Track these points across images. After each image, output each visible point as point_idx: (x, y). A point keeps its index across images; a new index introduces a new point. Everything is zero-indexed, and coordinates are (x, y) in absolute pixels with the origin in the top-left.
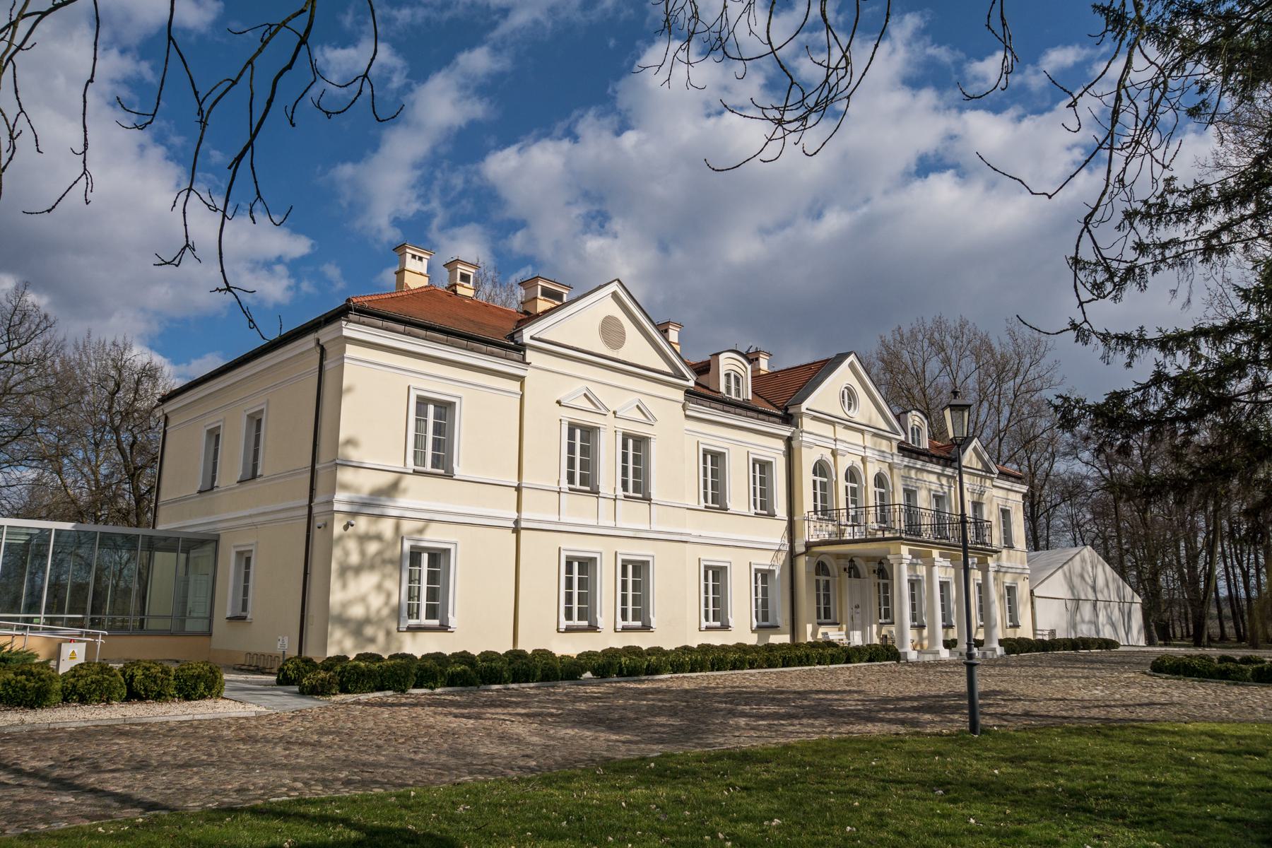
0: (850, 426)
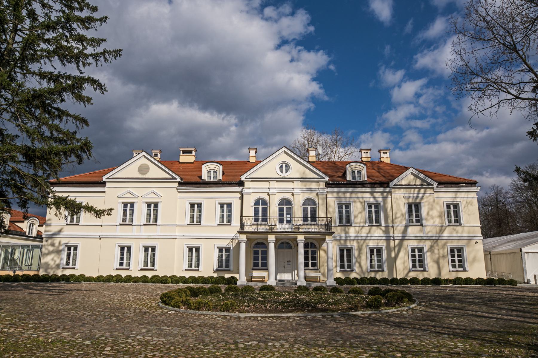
0: (291, 180)
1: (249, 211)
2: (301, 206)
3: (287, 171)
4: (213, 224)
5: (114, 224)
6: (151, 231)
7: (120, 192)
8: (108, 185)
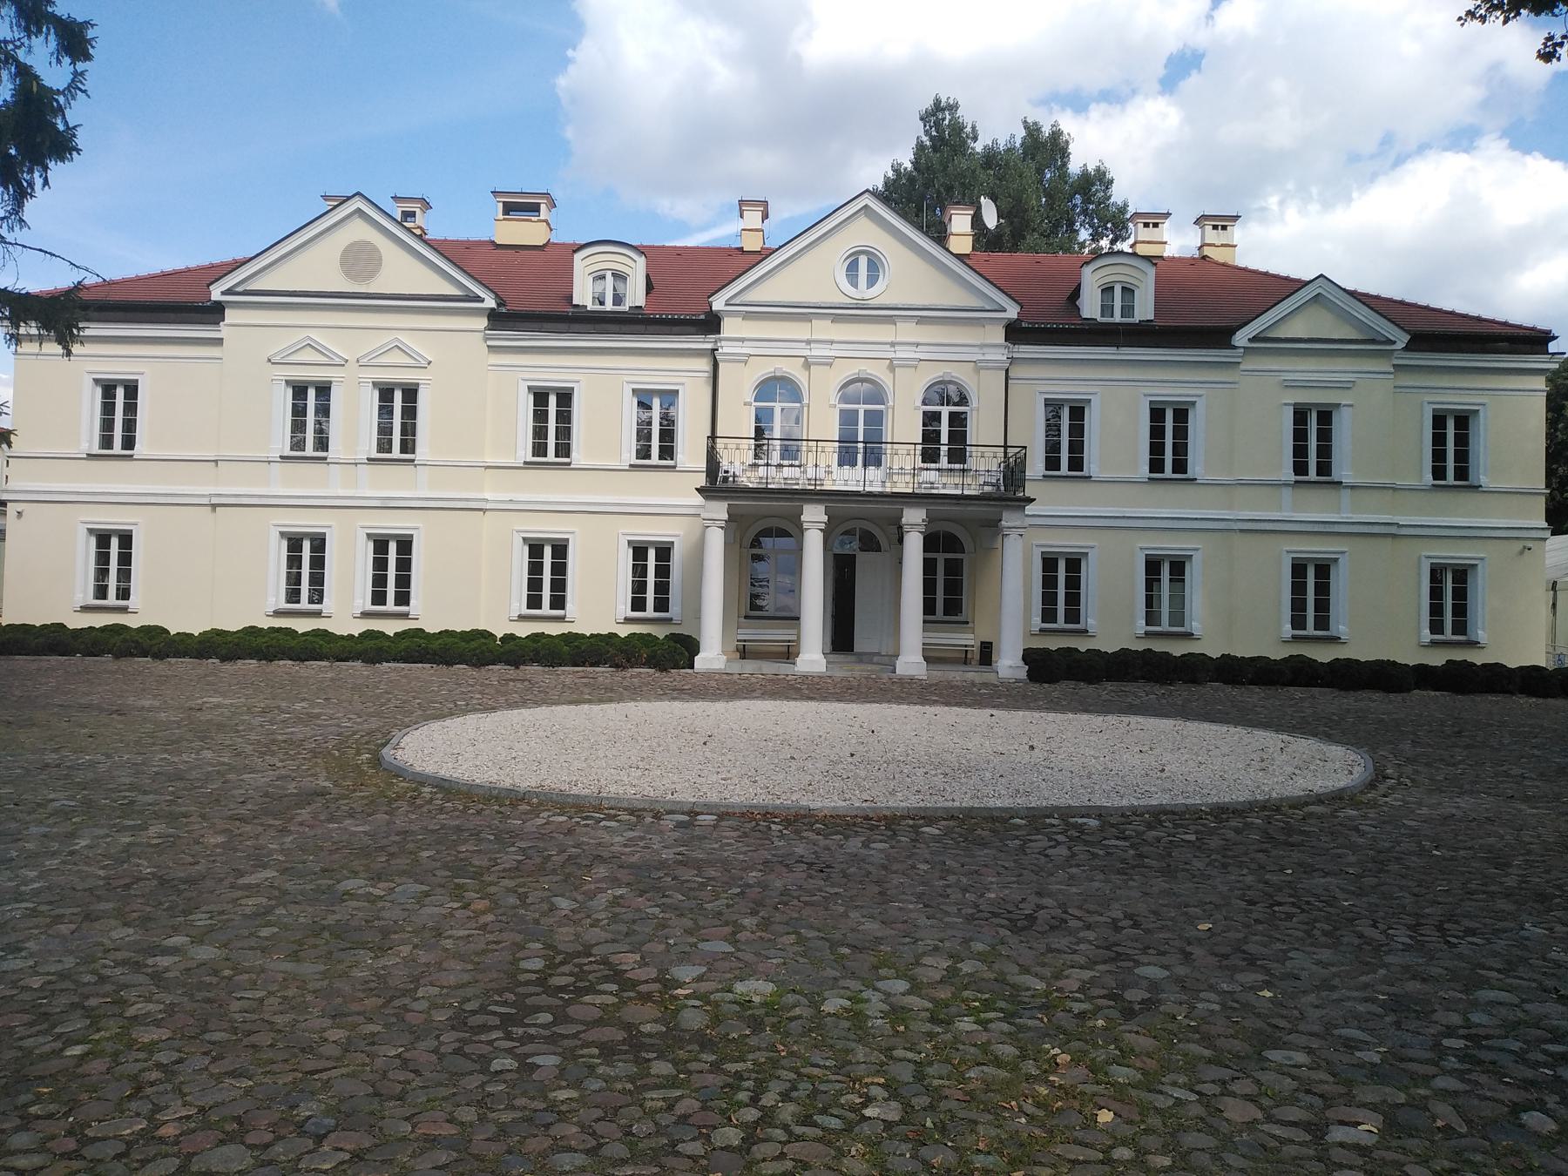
1: (738, 420)
2: (917, 408)
3: (872, 281)
4: (510, 461)
5: (262, 455)
6: (394, 483)
7: (279, 343)
8: (231, 315)
